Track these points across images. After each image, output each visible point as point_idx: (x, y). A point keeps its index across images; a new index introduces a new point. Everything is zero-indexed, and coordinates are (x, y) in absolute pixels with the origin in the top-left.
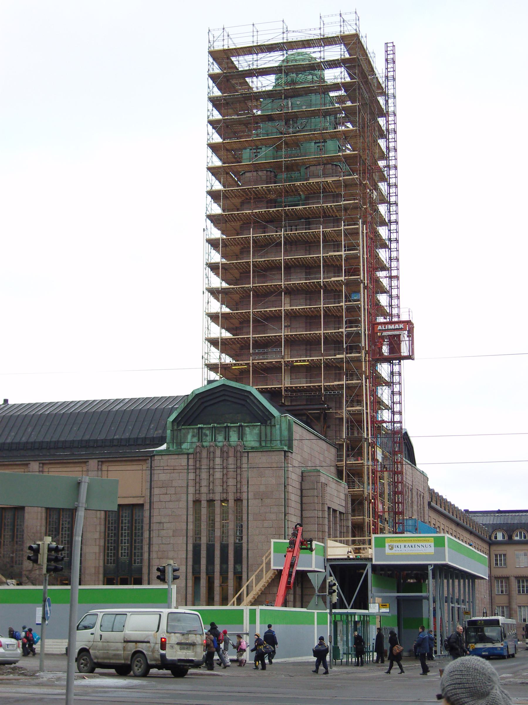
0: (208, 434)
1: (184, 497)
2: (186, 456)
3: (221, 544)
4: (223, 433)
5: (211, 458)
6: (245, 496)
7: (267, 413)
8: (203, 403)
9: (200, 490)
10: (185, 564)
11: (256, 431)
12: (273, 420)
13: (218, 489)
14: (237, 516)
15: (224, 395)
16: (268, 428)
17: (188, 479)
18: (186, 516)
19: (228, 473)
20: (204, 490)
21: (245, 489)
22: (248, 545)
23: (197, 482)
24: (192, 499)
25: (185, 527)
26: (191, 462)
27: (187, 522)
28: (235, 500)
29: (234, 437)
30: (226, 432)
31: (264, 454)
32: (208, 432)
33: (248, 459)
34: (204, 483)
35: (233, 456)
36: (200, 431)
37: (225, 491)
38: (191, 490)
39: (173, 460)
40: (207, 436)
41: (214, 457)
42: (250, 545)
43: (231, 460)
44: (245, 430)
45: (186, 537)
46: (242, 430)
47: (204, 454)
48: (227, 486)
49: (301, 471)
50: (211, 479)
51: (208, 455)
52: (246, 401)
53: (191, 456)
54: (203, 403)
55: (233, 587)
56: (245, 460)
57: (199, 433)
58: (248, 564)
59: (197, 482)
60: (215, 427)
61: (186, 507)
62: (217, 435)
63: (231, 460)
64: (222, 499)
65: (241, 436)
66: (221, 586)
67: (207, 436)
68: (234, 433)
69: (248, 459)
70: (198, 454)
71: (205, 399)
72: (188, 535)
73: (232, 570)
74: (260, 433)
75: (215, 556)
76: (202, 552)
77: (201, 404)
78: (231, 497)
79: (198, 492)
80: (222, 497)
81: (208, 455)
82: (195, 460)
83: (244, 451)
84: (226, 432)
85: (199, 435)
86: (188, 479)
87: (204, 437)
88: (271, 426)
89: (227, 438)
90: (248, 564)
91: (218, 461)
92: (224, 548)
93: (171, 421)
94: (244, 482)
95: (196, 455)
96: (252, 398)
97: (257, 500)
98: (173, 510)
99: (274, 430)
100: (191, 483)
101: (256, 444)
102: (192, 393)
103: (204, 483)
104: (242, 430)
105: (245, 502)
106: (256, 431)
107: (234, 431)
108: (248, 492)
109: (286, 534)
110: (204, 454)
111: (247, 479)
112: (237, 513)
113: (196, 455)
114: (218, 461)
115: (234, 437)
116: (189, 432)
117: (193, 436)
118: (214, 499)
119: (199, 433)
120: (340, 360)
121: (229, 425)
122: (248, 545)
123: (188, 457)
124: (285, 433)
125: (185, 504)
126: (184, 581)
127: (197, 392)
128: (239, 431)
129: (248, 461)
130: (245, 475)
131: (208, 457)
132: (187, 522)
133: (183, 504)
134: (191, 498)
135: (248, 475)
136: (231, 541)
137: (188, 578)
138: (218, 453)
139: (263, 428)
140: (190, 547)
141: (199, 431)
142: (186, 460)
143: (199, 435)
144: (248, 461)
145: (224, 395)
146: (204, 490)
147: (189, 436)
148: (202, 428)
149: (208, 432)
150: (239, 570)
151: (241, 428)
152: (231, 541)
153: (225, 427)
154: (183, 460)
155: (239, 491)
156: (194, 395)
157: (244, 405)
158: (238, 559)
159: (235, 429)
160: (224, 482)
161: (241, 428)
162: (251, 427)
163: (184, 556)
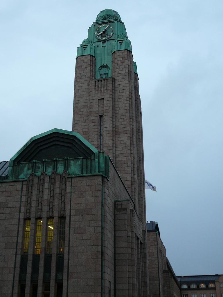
0: (40, 167)
1: (17, 215)
2: (21, 183)
3: (45, 255)
4: (52, 165)
5: (41, 184)
6: (67, 213)
7: (88, 151)
8: (39, 147)
9: (30, 210)
10: (13, 273)
11: (79, 163)
12: (93, 156)
13: (45, 208)
14: (60, 231)
15: (55, 141)
16: (89, 161)
17: (21, 201)
18: (17, 232)
19: (54, 195)
20: (33, 209)
21: (68, 207)
22: (69, 255)
23: (28, 204)
24: (23, 217)
25: (15, 241)
26: (25, 187)
27: (18, 236)
28: (59, 217)
29: (61, 169)
30: (54, 166)
31: (85, 178)
32: (40, 165)
33: (71, 184)
34: (34, 204)
35: (59, 181)
36: (34, 164)
37: (52, 210)
38: (23, 210)
39: (10, 187)
40: (39, 168)
41: (44, 183)
42: (70, 255)
43: (57, 185)
44: (70, 162)
45: (15, 249)
46: (68, 163)
47: (36, 180)
48: (53, 206)
49: (114, 201)
50: (40, 201)
51: (39, 181)
52: (72, 144)
53: (25, 183)
54: (39, 147)
55: (54, 294)
56: (69, 184)
57: (33, 166)
58: (68, 272)
59: (28, 204)
60: (46, 161)
61: (17, 224)
62: (47, 167)
63: (57, 185)
64: (48, 217)
65: (67, 166)
66: (43, 293)
67: (39, 168)
68: (61, 165)
69: (71, 184)
70: (31, 181)
71: (41, 144)
72: (18, 247)
73: (54, 278)
74: (82, 164)
75: (40, 266)
76: (28, 262)
77: (35, 145)
78: (56, 215)
79: (29, 211)
80: (48, 215)
81: (39, 181)
82: (28, 187)
83: (68, 177)
84: (54, 166)
85: (33, 168)
86: (21, 201)
87: (37, 170)
88: (91, 159)
89: (55, 168)
90: (68, 272)
91: (46, 185)
92: (48, 259)
93: (13, 160)
94: (68, 201)
95: (28, 182)
96: (76, 141)
97: (78, 216)
98: (7, 226)
99: (93, 163)
100: (23, 204)
101: (78, 173)
102: (31, 139)
103: (34, 204)
104: (68, 163)
105: (67, 219)
106: (79, 163)
107: (61, 164)
108: (70, 210)
109: (103, 197)
110: (36, 180)
111: (70, 199)
112: (60, 229)
113: (28, 182)
114: (46, 185)
115: (61, 169)
116: (25, 166)
117: (28, 169)
118: (41, 217)
119: (33, 166)
120: (141, 138)
121: (58, 159)
122: (69, 255)
123: (22, 183)
124: (103, 165)
125: (17, 221)
126: (11, 288)
127: (34, 139)
128: (65, 164)
129: (71, 185)
130: (68, 196)
131: (39, 183)
132: (18, 236)
133: (15, 221)
134: (22, 216)
135: (71, 196)
136: (54, 251)
137: (14, 286)
138: (47, 179)
139: (85, 160)
140: (19, 258)
141: (33, 165)
142: (20, 186)
143: (33, 168)
144: (71, 185)
145: (55, 141)
146: (33, 209)
147: (26, 169)
148: (35, 162)
149: (40, 165)
150: (61, 278)
151: (67, 161)
152: (54, 251)
153: (54, 161)
154: (18, 186)
155: (63, 209)
156: (32, 141)
157: (70, 147)
158: (60, 268)
159: (62, 162)
160: (51, 202)
161: (67, 161)
162: (75, 160)
163: (13, 266)
